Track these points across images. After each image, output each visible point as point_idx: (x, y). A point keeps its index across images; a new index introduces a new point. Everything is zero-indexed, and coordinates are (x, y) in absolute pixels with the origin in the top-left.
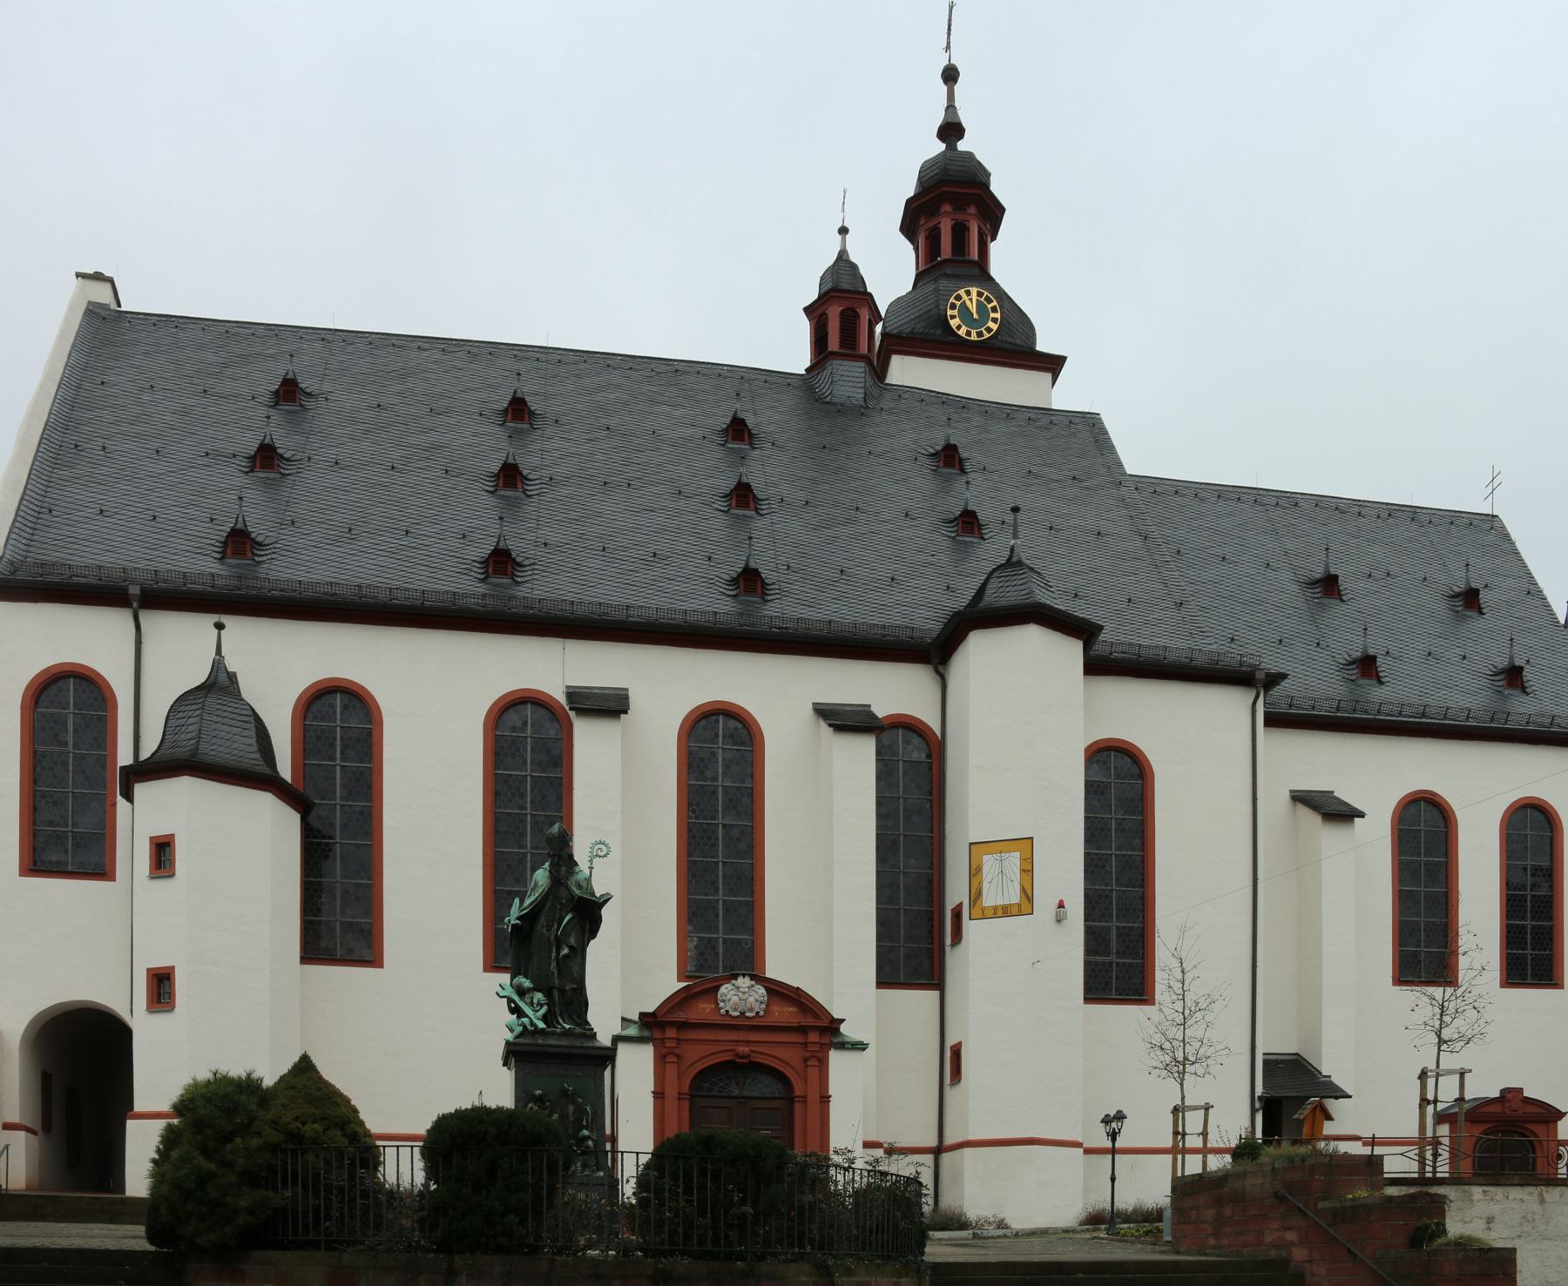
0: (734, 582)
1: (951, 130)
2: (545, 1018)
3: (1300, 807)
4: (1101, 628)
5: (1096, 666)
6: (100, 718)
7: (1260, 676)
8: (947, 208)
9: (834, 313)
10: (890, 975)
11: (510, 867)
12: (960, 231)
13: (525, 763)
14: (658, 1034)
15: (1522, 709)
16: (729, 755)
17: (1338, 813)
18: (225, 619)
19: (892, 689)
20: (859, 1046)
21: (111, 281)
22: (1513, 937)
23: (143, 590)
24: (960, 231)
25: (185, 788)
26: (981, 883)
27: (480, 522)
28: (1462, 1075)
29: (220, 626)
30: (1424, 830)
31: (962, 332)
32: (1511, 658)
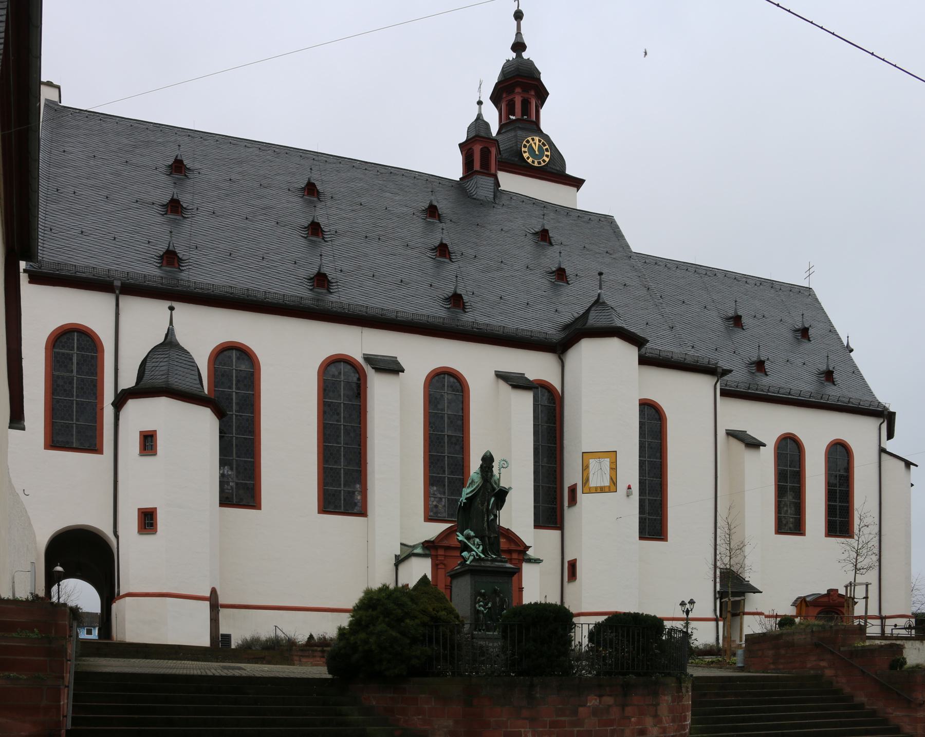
0: (448, 299)
1: (519, 47)
2: (483, 552)
3: (731, 438)
4: (648, 341)
5: (644, 361)
6: (92, 357)
7: (719, 370)
8: (518, 90)
9: (477, 149)
10: (539, 524)
11: (331, 454)
12: (526, 104)
13: (340, 396)
14: (433, 553)
15: (833, 393)
16: (450, 397)
17: (754, 444)
18: (175, 304)
19: (537, 366)
20: (537, 561)
21: (59, 88)
22: (831, 511)
23: (122, 284)
24: (526, 104)
25: (163, 404)
26: (588, 474)
27: (159, 233)
28: (867, 586)
29: (171, 309)
30: (790, 452)
31: (530, 161)
32: (828, 366)
